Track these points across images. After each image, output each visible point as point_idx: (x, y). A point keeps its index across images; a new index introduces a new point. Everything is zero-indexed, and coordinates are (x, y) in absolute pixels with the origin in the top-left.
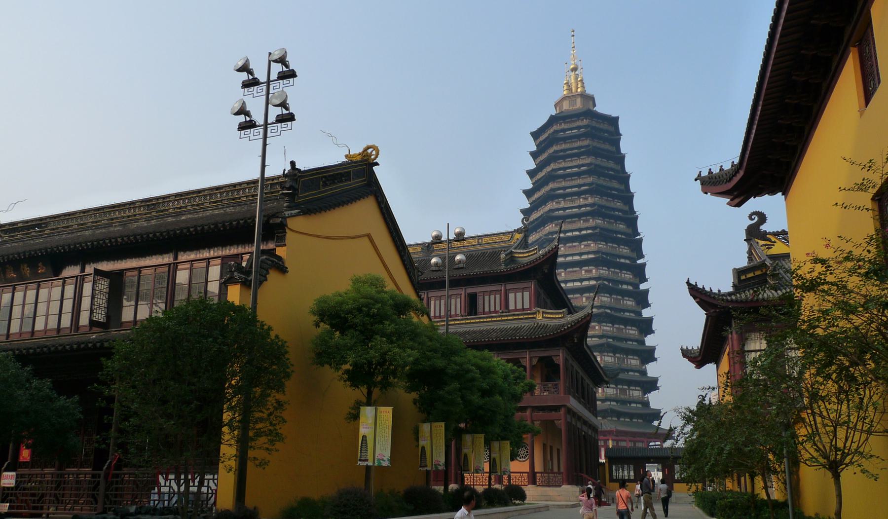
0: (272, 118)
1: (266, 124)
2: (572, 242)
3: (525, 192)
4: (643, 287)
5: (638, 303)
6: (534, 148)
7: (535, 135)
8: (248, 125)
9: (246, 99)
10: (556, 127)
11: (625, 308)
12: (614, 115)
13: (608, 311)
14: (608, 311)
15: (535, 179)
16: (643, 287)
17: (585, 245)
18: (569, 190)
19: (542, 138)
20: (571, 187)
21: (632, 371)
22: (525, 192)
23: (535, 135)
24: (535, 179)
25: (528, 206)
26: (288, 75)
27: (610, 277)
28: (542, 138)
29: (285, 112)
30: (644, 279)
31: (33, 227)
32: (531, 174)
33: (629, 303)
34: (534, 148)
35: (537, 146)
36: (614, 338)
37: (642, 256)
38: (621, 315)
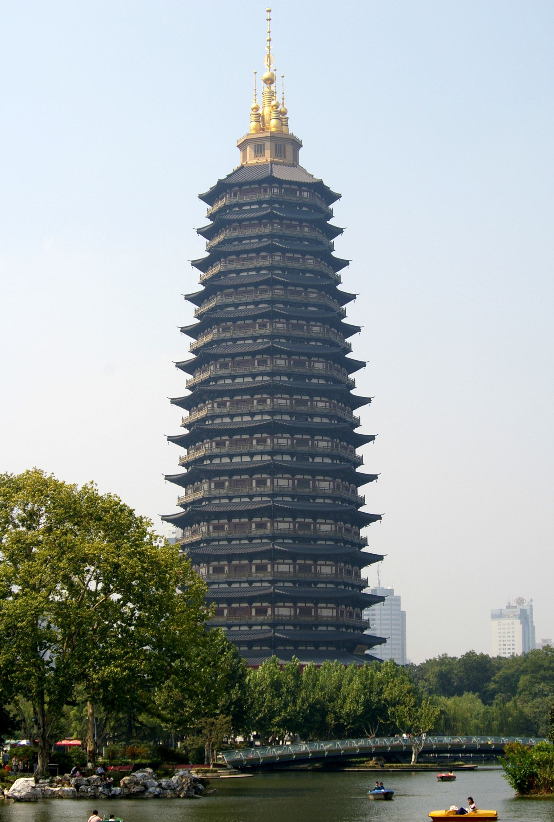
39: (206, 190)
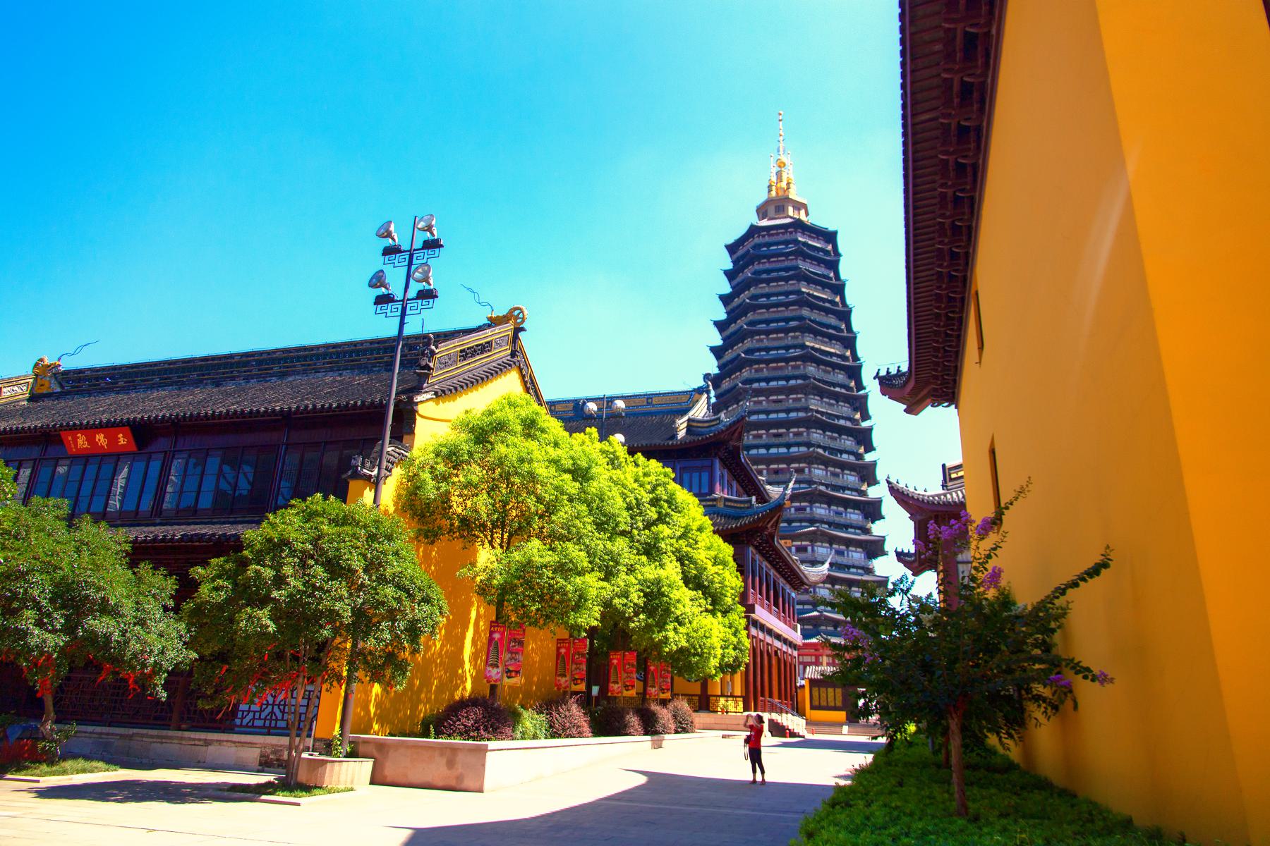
0: (412, 293)
1: (404, 303)
2: (777, 394)
3: (722, 298)
4: (869, 457)
5: (862, 479)
6: (730, 266)
7: (732, 249)
8: (382, 300)
9: (385, 268)
10: (757, 240)
11: (850, 563)
12: (831, 229)
13: (820, 451)
14: (820, 451)
15: (735, 256)
16: (869, 457)
17: (794, 400)
18: (774, 274)
19: (741, 252)
20: (777, 321)
21: (854, 567)
22: (722, 298)
23: (732, 249)
24: (730, 307)
25: (716, 371)
26: (432, 245)
27: (831, 519)
28: (741, 252)
29: (427, 287)
30: (870, 448)
31: (190, 370)
32: (725, 299)
33: (848, 443)
34: (730, 266)
35: (723, 339)
36: (830, 524)
37: (864, 388)
38: (838, 458)
39: (731, 241)
